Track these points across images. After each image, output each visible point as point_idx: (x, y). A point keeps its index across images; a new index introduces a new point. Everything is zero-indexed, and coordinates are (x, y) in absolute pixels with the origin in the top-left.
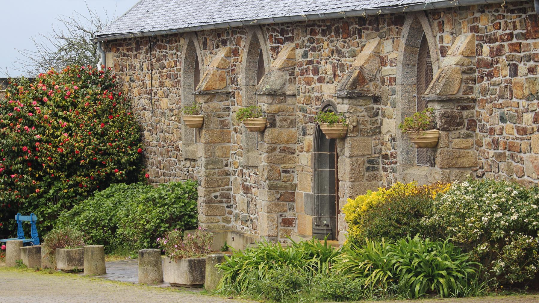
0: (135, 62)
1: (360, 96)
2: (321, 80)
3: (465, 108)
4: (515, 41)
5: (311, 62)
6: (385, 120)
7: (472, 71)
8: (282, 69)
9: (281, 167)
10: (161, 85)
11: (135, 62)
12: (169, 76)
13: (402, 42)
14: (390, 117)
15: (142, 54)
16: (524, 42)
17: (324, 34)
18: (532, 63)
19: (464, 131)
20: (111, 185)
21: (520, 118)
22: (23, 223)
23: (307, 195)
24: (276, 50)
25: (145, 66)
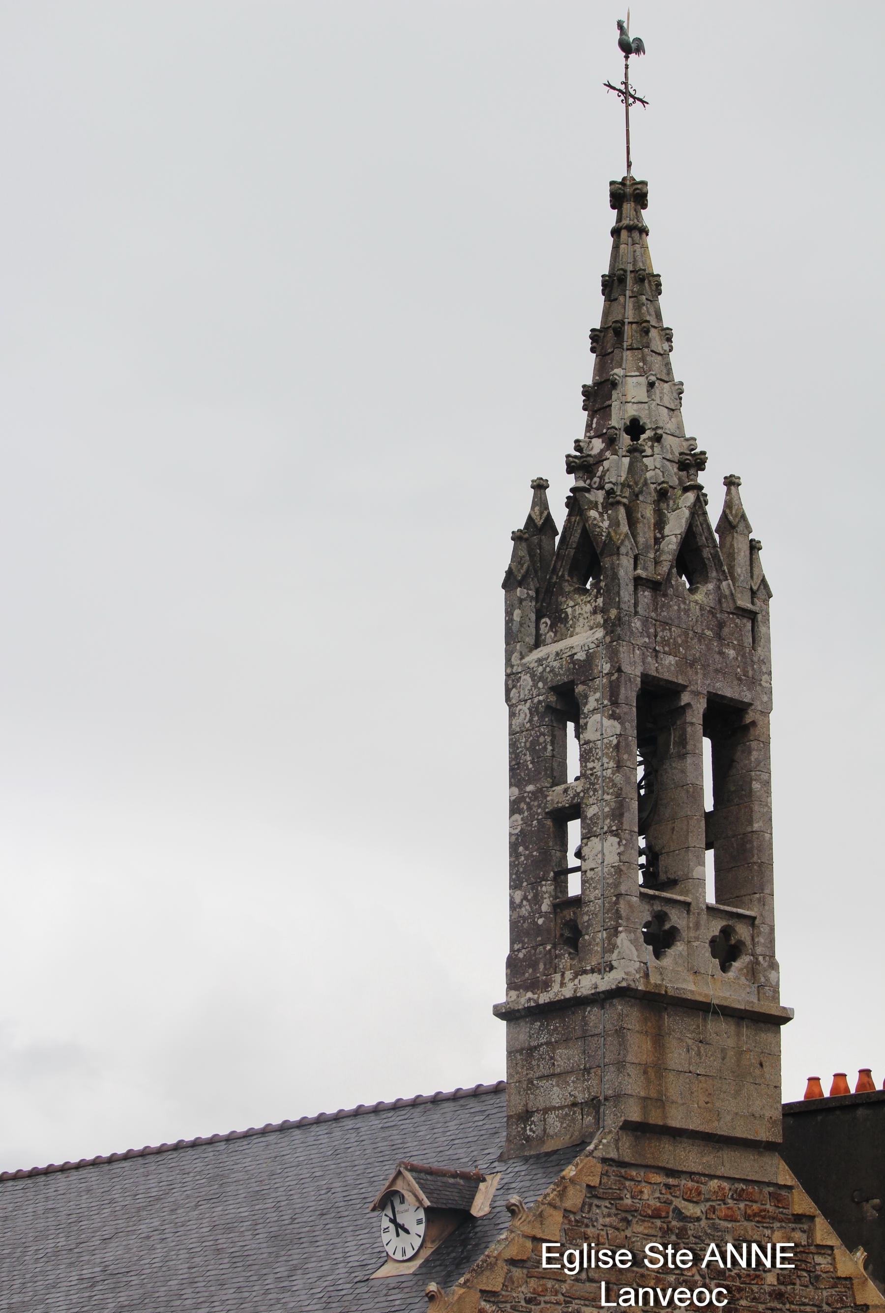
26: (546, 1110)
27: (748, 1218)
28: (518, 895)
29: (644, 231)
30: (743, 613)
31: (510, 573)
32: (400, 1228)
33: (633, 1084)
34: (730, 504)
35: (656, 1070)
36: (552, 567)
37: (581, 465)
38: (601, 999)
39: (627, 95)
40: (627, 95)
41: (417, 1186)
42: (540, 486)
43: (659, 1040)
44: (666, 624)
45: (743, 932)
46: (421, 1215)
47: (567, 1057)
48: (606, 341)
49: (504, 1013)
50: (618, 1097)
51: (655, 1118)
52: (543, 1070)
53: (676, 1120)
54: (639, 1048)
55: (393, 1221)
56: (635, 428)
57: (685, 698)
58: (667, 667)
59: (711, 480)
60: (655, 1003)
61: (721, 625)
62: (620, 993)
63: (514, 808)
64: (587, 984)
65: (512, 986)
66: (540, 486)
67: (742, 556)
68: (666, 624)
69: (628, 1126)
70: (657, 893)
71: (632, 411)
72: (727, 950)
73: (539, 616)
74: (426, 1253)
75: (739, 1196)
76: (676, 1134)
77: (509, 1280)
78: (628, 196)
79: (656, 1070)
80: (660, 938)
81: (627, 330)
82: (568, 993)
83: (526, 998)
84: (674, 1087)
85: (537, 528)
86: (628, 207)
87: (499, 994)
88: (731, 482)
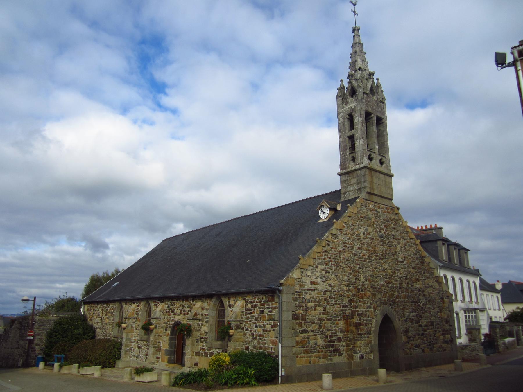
0: (96, 309)
1: (196, 319)
2: (174, 314)
3: (241, 323)
4: (262, 303)
5: (171, 309)
6: (203, 327)
7: (243, 312)
8: (160, 311)
9: (157, 341)
10: (106, 315)
11: (96, 309)
12: (109, 313)
13: (212, 303)
14: (204, 326)
15: (99, 306)
16: (266, 303)
17: (177, 301)
18: (270, 310)
19: (240, 330)
20: (519, 310)
21: (264, 326)
22: (57, 357)
23: (166, 350)
24: (156, 306)
25: (100, 310)
26: (350, 191)
27: (388, 213)
28: (342, 153)
29: (359, 36)
30: (381, 101)
31: (337, 95)
32: (324, 213)
33: (367, 184)
34: (378, 83)
35: (371, 182)
36: (348, 93)
37: (350, 76)
38: (360, 169)
39: (354, 12)
40: (354, 12)
41: (73, 284)
42: (342, 81)
43: (372, 176)
44: (369, 101)
45: (384, 159)
46: (328, 209)
47: (353, 181)
48: (353, 55)
49: (339, 174)
50: (365, 188)
51: (372, 192)
52: (348, 184)
53: (376, 193)
54: (368, 178)
55: (322, 211)
56: (360, 69)
57: (373, 115)
58: (370, 109)
59: (375, 77)
60: (371, 169)
61: (378, 104)
62: (365, 167)
63: (340, 137)
64: (358, 167)
65: (340, 169)
66: (342, 81)
67: (380, 92)
68: (369, 101)
69: (368, 193)
70: (109, 290)
71: (359, 66)
72: (382, 163)
73: (343, 103)
74: (329, 217)
75: (387, 208)
76: (376, 195)
77: (348, 221)
78: (355, 30)
79: (371, 182)
80: (371, 159)
81: (358, 52)
82: (353, 168)
83: (344, 171)
84: (375, 186)
85: (341, 89)
86: (356, 32)
87: (338, 171)
88: (378, 79)
